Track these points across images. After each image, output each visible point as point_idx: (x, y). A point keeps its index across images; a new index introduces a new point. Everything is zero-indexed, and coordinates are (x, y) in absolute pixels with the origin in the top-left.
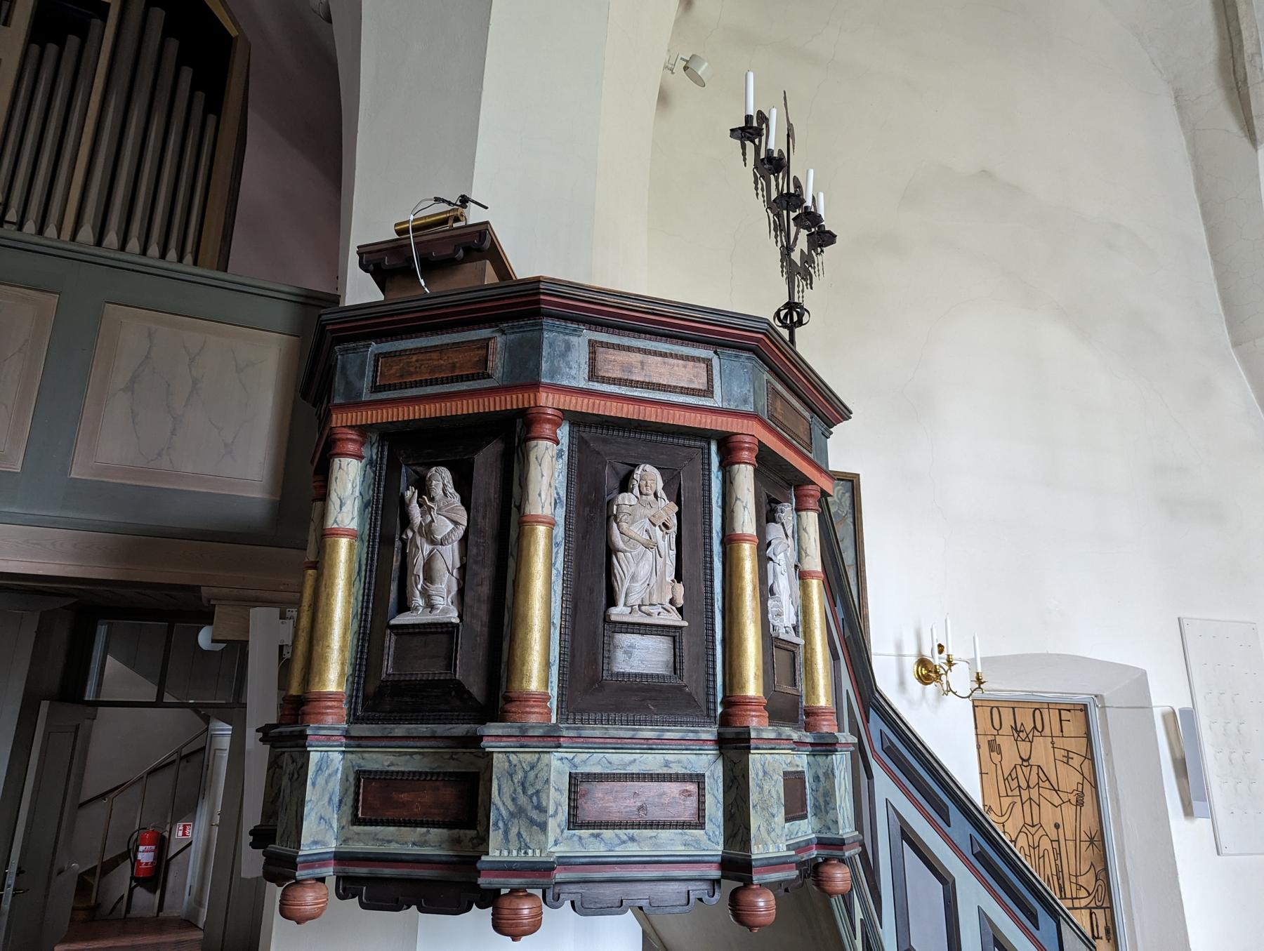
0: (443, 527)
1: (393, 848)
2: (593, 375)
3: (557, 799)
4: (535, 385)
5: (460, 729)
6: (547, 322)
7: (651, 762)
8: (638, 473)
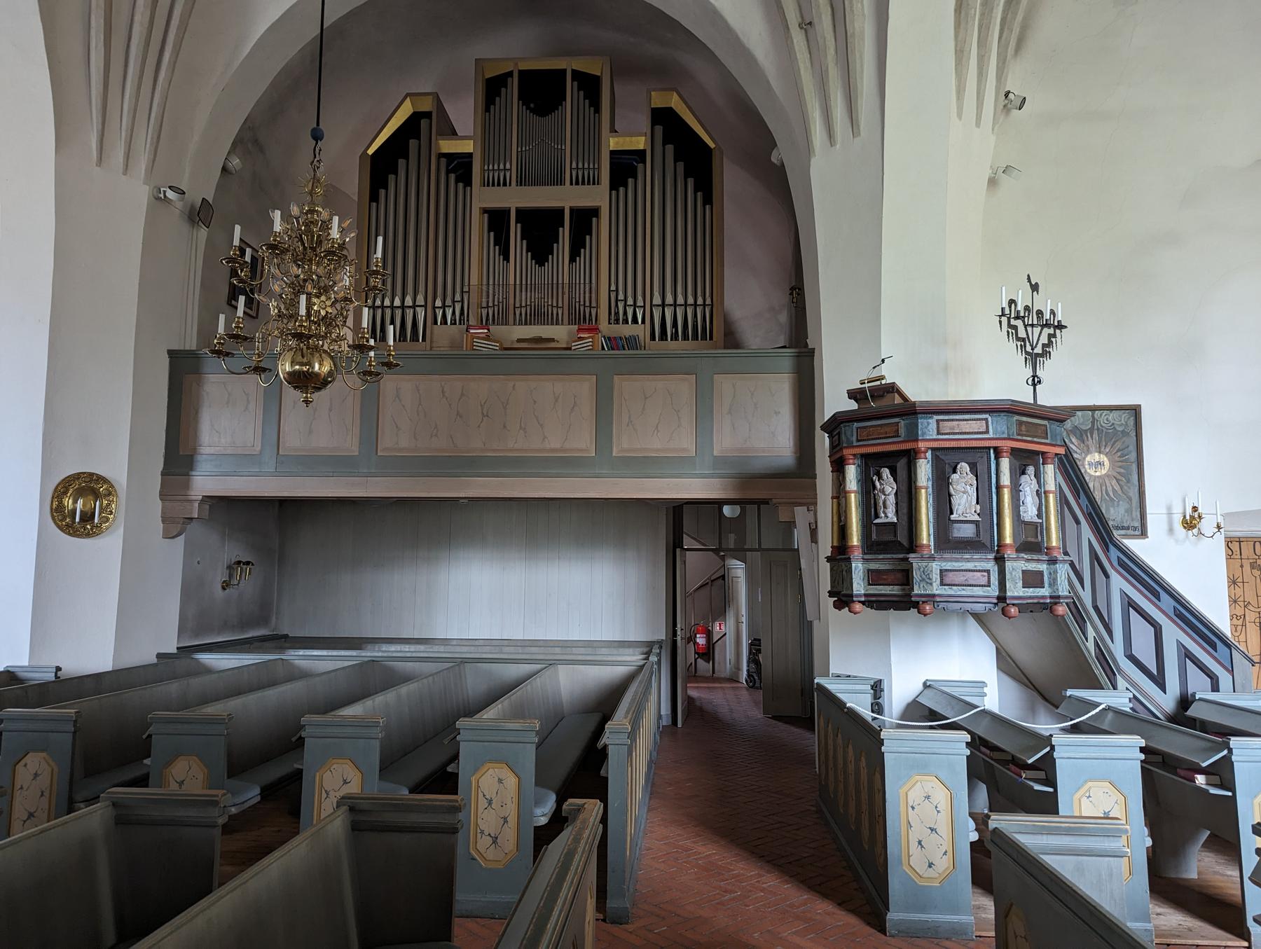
0: (888, 489)
2: (939, 433)
3: (936, 577)
4: (917, 440)
5: (901, 556)
7: (970, 566)
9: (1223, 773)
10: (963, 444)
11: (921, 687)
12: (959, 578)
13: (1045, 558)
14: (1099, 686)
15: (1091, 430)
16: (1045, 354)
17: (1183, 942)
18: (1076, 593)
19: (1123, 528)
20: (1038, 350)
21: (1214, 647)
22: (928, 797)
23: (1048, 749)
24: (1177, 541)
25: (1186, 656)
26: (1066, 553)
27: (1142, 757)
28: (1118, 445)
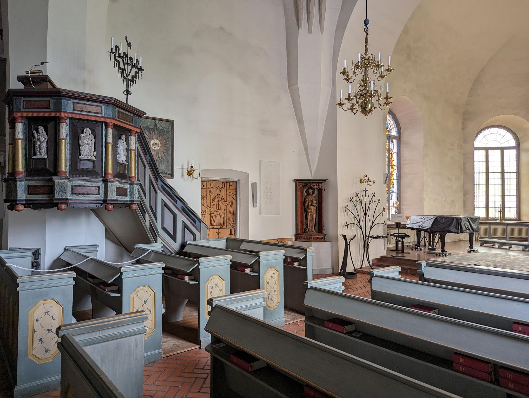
0: (42, 139)
1: (37, 198)
2: (74, 110)
3: (69, 189)
5: (49, 177)
6: (63, 98)
7: (89, 184)
8: (85, 130)
9: (195, 275)
10: (88, 118)
11: (63, 250)
12: (83, 190)
13: (128, 182)
14: (149, 242)
15: (154, 128)
16: (133, 81)
17: (174, 353)
18: (142, 200)
19: (165, 174)
20: (130, 77)
21: (195, 222)
22: (47, 313)
23: (119, 274)
24: (184, 180)
25: (185, 227)
26: (138, 180)
27: (163, 272)
28: (165, 137)
